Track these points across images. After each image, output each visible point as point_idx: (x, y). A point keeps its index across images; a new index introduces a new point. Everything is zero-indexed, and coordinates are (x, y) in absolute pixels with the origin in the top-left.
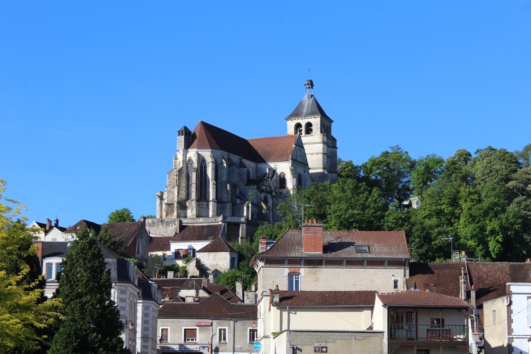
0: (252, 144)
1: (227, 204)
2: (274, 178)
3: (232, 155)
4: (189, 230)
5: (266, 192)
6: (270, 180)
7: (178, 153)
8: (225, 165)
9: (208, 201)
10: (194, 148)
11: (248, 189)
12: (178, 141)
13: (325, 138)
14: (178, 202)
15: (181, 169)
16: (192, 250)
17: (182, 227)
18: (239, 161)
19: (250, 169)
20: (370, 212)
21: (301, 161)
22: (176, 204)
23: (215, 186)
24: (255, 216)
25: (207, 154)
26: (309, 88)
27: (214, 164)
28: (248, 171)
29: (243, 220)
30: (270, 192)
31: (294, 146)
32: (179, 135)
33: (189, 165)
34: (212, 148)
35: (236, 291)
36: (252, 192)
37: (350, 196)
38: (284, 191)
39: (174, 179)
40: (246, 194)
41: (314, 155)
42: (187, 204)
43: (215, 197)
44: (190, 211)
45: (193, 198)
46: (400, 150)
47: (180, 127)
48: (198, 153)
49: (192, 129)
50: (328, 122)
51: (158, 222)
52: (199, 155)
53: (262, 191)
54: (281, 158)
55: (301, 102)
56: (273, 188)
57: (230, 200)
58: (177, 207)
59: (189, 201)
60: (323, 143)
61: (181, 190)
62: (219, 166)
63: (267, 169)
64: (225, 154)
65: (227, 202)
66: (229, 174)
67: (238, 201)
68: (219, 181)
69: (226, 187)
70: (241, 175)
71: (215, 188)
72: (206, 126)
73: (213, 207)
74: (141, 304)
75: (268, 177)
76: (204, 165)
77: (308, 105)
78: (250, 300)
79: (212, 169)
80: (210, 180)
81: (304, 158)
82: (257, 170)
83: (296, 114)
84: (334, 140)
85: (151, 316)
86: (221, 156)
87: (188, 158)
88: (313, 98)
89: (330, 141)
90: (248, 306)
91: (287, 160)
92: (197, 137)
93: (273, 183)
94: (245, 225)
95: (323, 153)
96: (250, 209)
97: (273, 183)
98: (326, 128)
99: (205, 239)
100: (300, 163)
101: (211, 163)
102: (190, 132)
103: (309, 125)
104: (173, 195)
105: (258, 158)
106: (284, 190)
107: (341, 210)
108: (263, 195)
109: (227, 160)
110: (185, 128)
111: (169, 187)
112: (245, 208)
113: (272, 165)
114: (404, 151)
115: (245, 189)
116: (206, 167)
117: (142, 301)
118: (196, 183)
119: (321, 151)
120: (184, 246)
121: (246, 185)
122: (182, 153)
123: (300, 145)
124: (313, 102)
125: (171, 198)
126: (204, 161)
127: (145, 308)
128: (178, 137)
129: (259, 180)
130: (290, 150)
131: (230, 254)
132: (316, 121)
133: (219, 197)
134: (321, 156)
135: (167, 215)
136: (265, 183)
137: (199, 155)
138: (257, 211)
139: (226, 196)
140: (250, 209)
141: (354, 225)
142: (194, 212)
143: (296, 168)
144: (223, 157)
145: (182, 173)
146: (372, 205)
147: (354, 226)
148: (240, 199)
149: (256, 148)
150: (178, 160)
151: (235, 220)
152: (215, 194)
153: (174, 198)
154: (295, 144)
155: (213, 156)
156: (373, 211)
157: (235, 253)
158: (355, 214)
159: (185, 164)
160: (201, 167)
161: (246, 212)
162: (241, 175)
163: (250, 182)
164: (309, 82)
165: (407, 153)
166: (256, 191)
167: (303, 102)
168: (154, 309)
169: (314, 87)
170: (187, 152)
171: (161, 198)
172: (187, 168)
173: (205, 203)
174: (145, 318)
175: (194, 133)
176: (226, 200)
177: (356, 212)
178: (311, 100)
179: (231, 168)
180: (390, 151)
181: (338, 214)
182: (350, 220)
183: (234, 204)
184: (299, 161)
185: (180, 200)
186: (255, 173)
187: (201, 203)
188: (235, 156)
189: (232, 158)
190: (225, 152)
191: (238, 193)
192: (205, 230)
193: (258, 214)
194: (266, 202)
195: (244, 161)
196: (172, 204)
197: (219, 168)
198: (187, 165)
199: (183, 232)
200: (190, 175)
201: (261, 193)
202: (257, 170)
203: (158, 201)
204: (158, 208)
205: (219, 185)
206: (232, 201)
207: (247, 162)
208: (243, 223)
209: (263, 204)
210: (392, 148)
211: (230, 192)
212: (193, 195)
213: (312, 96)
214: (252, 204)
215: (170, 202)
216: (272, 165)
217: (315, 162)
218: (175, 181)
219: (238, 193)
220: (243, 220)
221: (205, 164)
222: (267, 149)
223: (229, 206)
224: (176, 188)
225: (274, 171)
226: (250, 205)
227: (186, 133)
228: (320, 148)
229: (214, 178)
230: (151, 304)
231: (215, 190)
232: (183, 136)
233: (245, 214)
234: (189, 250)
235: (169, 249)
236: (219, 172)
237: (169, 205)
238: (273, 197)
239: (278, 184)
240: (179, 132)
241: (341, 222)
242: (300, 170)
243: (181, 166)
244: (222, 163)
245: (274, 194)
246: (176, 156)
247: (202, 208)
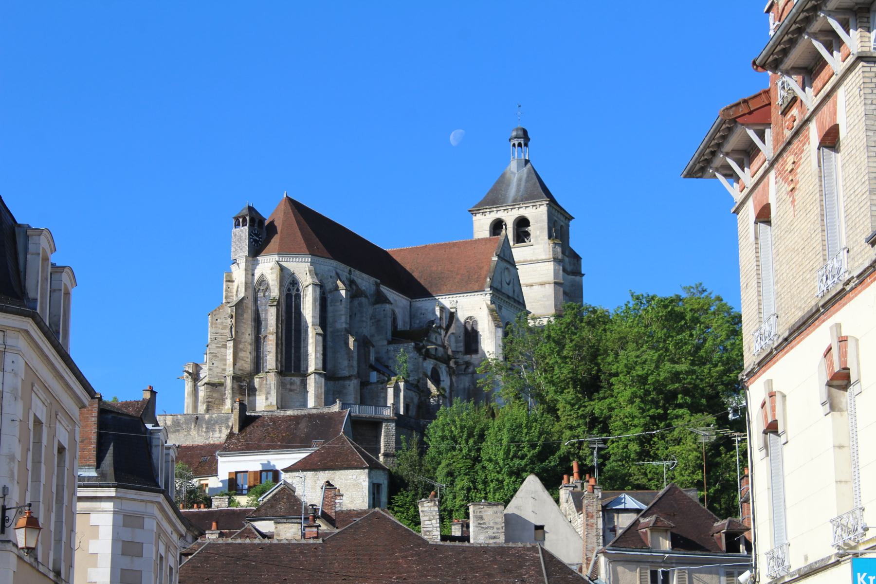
0: (398, 260)
1: (347, 382)
2: (452, 330)
3: (357, 272)
4: (263, 426)
5: (436, 358)
6: (443, 332)
7: (234, 268)
8: (343, 293)
9: (304, 375)
10: (270, 253)
11: (396, 351)
12: (233, 239)
13: (559, 249)
14: (234, 378)
15: (241, 301)
16: (270, 474)
17: (246, 421)
18: (373, 288)
19: (397, 311)
20: (714, 370)
21: (511, 294)
22: (229, 382)
23: (320, 338)
24: (413, 412)
25: (302, 268)
26: (520, 145)
27: (318, 289)
28: (393, 312)
29: (388, 413)
30: (446, 360)
31: (495, 259)
32: (237, 225)
33: (260, 295)
34: (312, 254)
35: (419, 523)
36: (404, 356)
37: (660, 334)
38: (474, 358)
39: (224, 328)
40: (390, 363)
41: (536, 287)
42: (257, 381)
43: (320, 365)
44: (264, 397)
45: (269, 367)
46: (706, 294)
47: (241, 208)
48: (280, 266)
49: (267, 214)
50: (563, 218)
51: (187, 422)
52: (282, 269)
53: (427, 355)
54: (467, 286)
55: (503, 176)
56: (450, 352)
57: (355, 373)
58: (233, 389)
59: (261, 375)
60: (555, 260)
61: (242, 350)
62: (329, 297)
63: (437, 309)
64: (344, 269)
65: (349, 378)
66: (352, 316)
67: (374, 376)
68: (329, 330)
69: (347, 344)
70: (379, 321)
71: (321, 344)
72: (297, 207)
73: (317, 387)
74: (109, 506)
75: (440, 327)
76: (294, 293)
77: (520, 180)
78: (490, 532)
79: (314, 300)
80: (310, 325)
81: (516, 289)
82: (413, 314)
83: (493, 200)
84: (576, 258)
85: (150, 552)
86: (334, 274)
87: (256, 277)
88: (529, 165)
89: (567, 259)
90: (483, 550)
91: (481, 290)
92: (279, 229)
93: (449, 341)
94: (393, 425)
95: (555, 283)
96: (402, 394)
97: (451, 342)
98: (559, 228)
99: (303, 444)
100: (509, 297)
101: (310, 288)
102: (262, 220)
103: (522, 223)
104: (221, 363)
105: (415, 289)
106: (474, 356)
107: (644, 363)
108: (429, 365)
109: (347, 282)
110: (251, 209)
111: (213, 346)
112: (390, 392)
113: (447, 301)
114: (713, 296)
115: (388, 351)
116: (298, 296)
117: (112, 492)
118: (277, 333)
119: (551, 278)
120: (251, 463)
121: (389, 343)
122: (243, 265)
123: (507, 260)
124: (529, 174)
125: (219, 370)
126: (294, 282)
127: (126, 521)
128: (234, 230)
129: (417, 333)
130: (486, 268)
131: (370, 476)
132: (537, 215)
133: (329, 367)
134: (550, 290)
135: (208, 410)
136: (433, 337)
137: (282, 269)
138: (416, 400)
139: (346, 363)
140: (402, 394)
141: (680, 399)
142: (273, 399)
143: (500, 308)
144: (338, 277)
145: (244, 312)
146: (716, 357)
147: (680, 401)
148: (378, 371)
149: (408, 268)
150: (235, 285)
151: (369, 412)
152: (321, 357)
153: (224, 370)
154: (498, 256)
155: (316, 273)
156: (720, 368)
157: (381, 472)
158: (681, 373)
159: (250, 291)
160: (289, 296)
161: (393, 399)
162: (379, 321)
163: (398, 336)
164: (521, 133)
165: (719, 299)
166: (414, 354)
167: (508, 175)
168: (161, 531)
169: (530, 143)
170: (255, 264)
171: (195, 377)
172: (256, 299)
173: (297, 380)
174: (126, 562)
175: (272, 223)
176: (346, 373)
177: (683, 367)
178: (525, 170)
179: (356, 303)
180: (684, 295)
181: (640, 373)
182: (671, 387)
183: (364, 384)
184: (508, 298)
185: (239, 373)
186: (408, 320)
187: (288, 378)
188: (364, 275)
189: (359, 281)
190: (343, 266)
191: (372, 358)
192: (302, 425)
193: (419, 407)
194: (437, 382)
195: (384, 289)
196: (221, 384)
197: (329, 300)
198: (256, 292)
199: (248, 429)
200: (263, 316)
201: (425, 359)
202: (413, 314)
203: (188, 386)
204: (188, 401)
205: (329, 338)
206: (358, 376)
207: (391, 294)
208: (388, 420)
209: (429, 383)
210: (687, 289)
211: (355, 355)
212: (270, 360)
213: (527, 162)
214: (406, 382)
215: (216, 381)
216: (447, 301)
217: (540, 298)
218: (227, 331)
219: (372, 358)
220: (388, 413)
221: (298, 290)
222: (434, 269)
223: (352, 386)
224: (230, 344)
225: (452, 316)
226: (402, 385)
227: (252, 220)
228: (547, 271)
229: (318, 321)
230: (147, 503)
231: (320, 349)
232: (246, 228)
233: (390, 401)
234: (264, 474)
235: (214, 472)
236: (330, 309)
237: (214, 386)
238: (451, 372)
239: (462, 344)
240: (237, 219)
241: (647, 393)
242: (508, 313)
243: (242, 294)
244: (337, 288)
245: (452, 364)
246: (230, 273)
247: (291, 390)
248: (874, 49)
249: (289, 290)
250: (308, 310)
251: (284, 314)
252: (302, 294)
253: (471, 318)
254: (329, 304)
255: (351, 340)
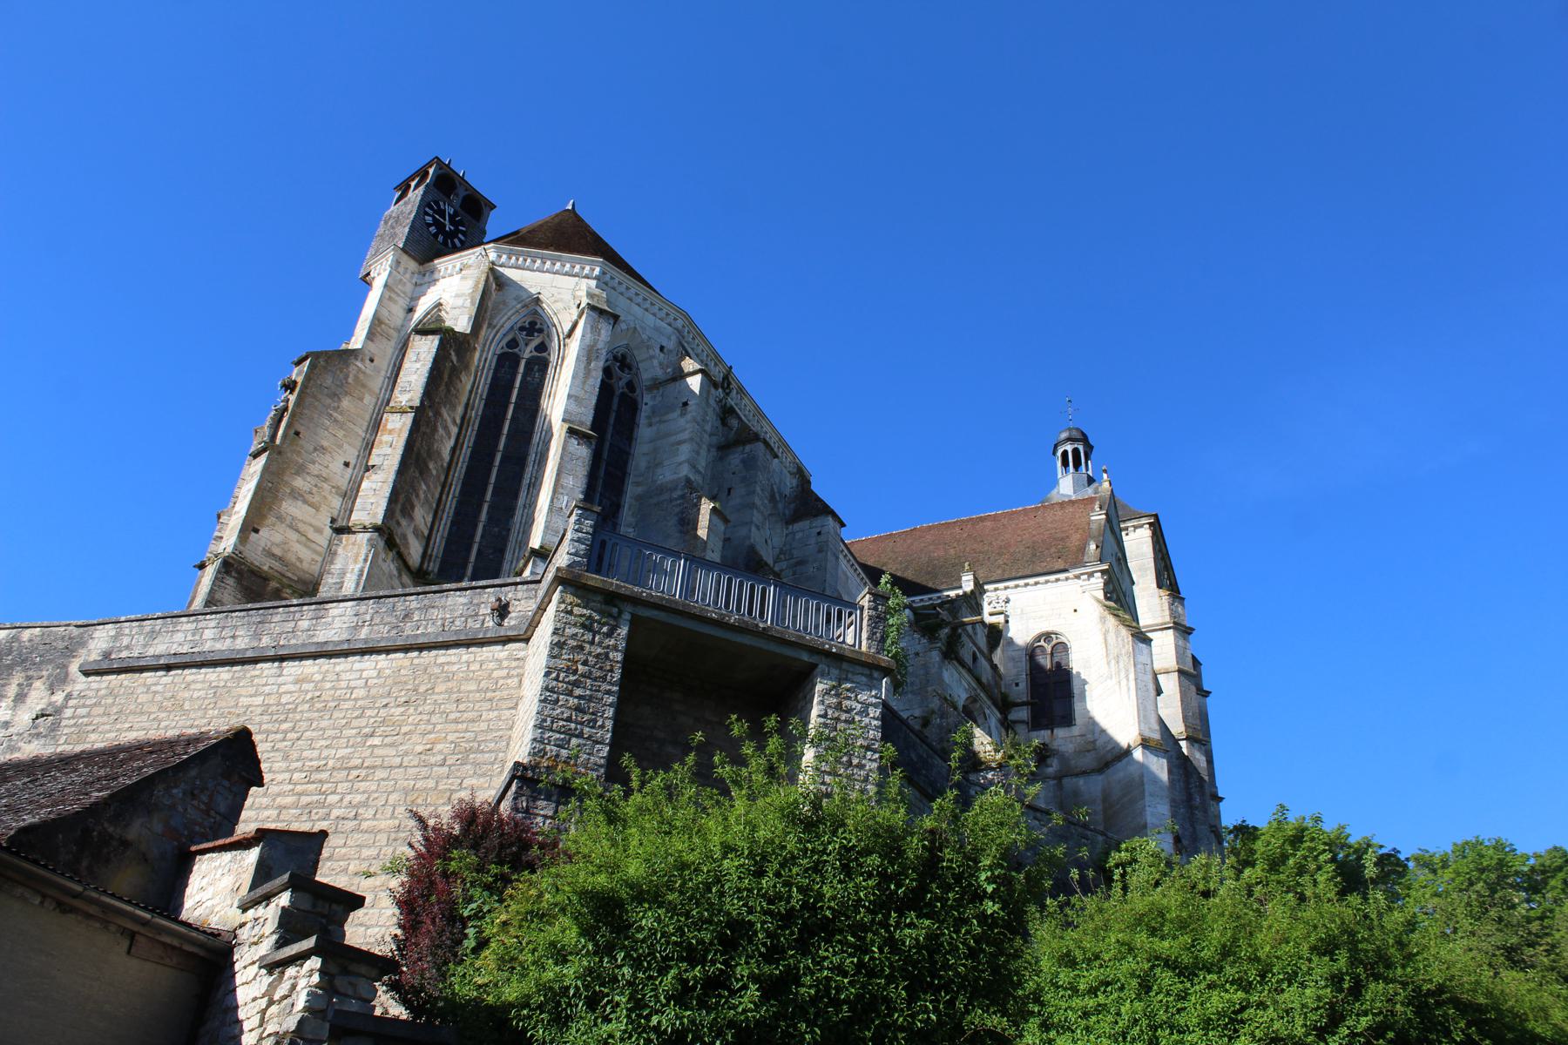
38: (1063, 739)
69: (689, 523)
70: (801, 563)
76: (527, 353)
95: (1181, 672)
106: (1060, 733)
164: (1079, 436)
170: (426, 278)
179: (735, 459)
248: (913, 1035)
249: (513, 343)
250: (562, 397)
251: (479, 405)
252: (553, 358)
253: (1047, 636)
254: (642, 419)
255: (706, 506)
